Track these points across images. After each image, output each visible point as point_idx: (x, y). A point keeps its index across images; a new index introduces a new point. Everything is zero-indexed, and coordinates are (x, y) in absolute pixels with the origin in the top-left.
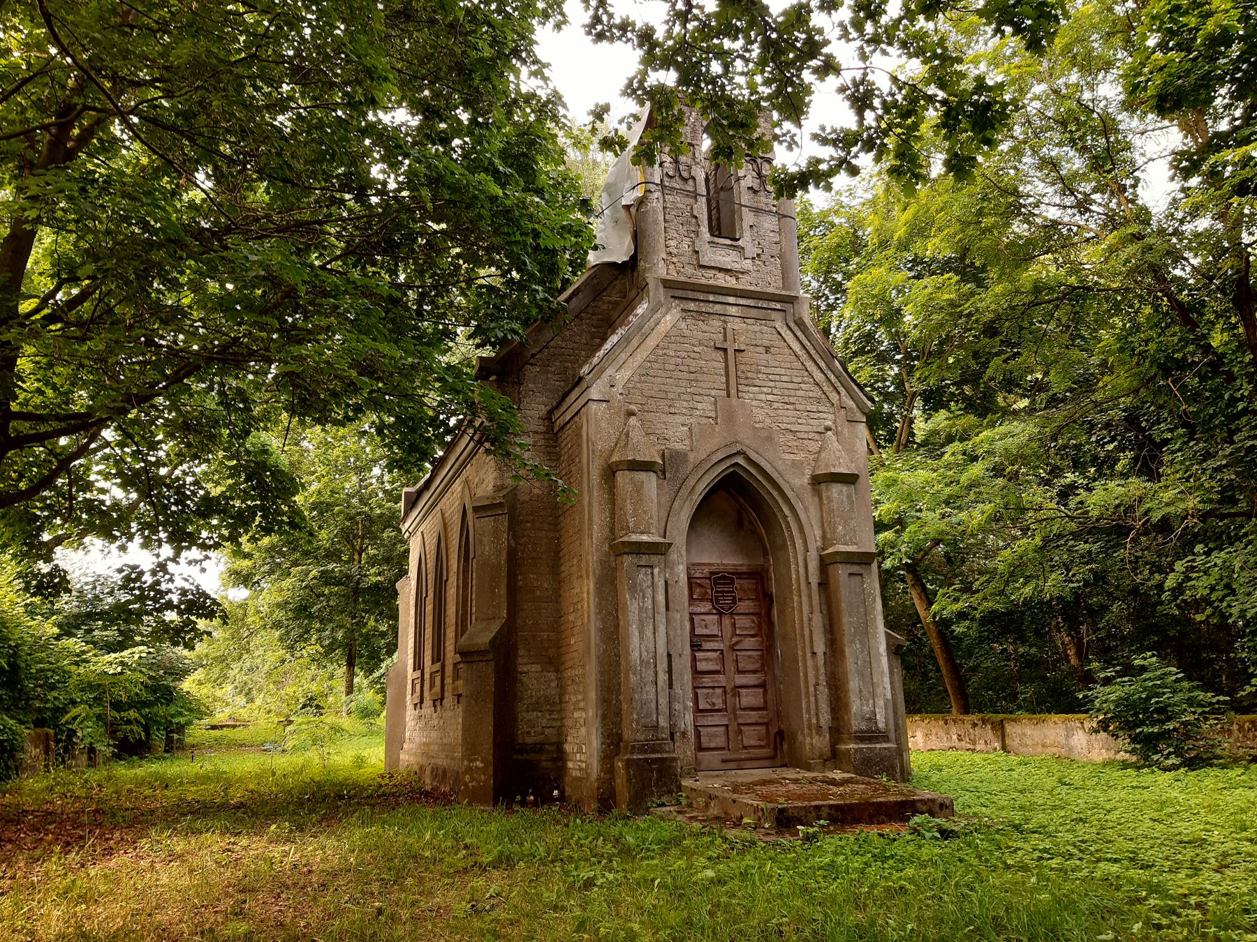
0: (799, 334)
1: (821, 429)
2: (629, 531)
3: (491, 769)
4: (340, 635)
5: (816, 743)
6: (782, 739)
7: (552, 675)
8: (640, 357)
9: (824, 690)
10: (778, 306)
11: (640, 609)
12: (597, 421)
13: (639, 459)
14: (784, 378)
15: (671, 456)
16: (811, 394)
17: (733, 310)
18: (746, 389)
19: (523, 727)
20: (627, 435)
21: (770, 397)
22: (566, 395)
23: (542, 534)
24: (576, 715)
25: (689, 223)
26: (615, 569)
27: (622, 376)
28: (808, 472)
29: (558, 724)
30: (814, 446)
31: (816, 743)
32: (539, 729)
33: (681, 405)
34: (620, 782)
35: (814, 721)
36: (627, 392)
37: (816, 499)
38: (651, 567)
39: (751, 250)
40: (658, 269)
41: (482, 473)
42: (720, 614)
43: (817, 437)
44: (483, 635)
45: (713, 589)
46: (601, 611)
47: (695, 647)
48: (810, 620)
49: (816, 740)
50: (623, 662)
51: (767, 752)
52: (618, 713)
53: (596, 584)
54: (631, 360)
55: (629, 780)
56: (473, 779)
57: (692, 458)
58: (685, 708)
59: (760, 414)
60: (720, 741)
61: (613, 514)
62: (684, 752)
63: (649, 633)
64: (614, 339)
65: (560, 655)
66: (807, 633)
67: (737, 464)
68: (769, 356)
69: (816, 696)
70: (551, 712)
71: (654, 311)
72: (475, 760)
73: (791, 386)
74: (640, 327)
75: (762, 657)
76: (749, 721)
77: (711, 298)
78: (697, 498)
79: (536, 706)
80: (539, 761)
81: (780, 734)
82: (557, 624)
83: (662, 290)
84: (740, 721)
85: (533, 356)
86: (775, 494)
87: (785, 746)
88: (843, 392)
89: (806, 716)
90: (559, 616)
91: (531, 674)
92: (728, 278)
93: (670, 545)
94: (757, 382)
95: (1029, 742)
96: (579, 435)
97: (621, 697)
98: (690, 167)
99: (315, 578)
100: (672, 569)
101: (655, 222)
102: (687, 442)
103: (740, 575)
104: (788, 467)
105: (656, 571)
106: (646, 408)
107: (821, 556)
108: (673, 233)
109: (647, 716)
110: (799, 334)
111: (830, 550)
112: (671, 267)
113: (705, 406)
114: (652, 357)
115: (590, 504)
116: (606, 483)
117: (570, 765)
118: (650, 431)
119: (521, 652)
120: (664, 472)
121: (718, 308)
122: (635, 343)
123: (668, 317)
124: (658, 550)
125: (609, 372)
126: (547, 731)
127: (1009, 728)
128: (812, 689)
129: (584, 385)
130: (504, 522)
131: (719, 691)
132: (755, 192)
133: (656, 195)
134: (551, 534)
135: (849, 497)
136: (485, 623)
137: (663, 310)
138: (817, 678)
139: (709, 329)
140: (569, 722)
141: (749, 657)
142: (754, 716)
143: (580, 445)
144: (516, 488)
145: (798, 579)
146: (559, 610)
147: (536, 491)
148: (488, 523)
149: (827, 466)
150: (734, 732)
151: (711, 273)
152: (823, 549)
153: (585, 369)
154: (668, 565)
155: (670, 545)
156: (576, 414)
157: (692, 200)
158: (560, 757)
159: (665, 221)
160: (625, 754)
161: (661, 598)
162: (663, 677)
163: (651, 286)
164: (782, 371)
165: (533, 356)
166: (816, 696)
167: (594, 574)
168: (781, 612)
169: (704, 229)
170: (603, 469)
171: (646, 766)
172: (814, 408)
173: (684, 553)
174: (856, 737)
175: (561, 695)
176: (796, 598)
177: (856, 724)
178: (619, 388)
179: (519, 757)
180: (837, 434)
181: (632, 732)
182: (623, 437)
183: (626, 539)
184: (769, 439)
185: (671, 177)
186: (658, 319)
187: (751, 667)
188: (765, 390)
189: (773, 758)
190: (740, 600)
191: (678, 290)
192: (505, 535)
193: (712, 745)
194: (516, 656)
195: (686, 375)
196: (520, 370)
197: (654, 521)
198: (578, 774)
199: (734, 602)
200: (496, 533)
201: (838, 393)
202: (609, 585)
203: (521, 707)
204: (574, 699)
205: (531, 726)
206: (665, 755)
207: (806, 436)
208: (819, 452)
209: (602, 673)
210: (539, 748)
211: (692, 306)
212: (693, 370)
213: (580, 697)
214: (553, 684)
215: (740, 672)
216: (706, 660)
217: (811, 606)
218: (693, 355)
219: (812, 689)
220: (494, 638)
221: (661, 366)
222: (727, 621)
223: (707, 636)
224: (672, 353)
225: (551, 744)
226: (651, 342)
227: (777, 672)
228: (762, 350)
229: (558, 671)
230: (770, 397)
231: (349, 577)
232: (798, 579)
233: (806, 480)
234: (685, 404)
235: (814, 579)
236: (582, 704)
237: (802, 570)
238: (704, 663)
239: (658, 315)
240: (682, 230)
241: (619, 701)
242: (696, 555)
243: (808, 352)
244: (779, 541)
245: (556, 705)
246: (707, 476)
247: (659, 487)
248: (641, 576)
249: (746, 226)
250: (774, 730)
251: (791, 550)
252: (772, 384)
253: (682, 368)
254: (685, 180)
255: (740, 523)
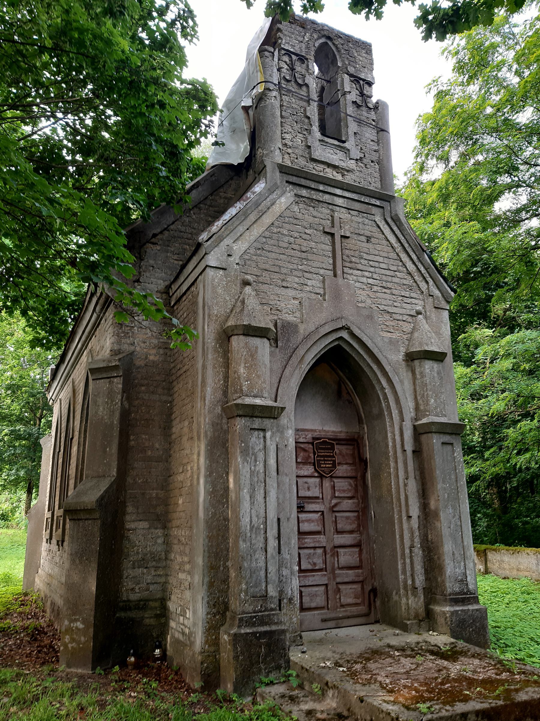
0: (395, 228)
1: (413, 313)
2: (243, 394)
3: (91, 630)
4: (22, 473)
5: (412, 603)
6: (375, 596)
7: (160, 532)
8: (257, 231)
9: (418, 552)
10: (378, 203)
11: (252, 473)
12: (214, 288)
13: (254, 324)
14: (382, 266)
15: (283, 326)
16: (405, 282)
17: (340, 201)
18: (351, 271)
19: (127, 584)
20: (243, 302)
21: (370, 281)
22: (183, 267)
23: (156, 397)
24: (182, 576)
25: (303, 122)
26: (227, 432)
27: (239, 248)
28: (403, 350)
29: (163, 580)
30: (408, 327)
31: (412, 603)
32: (144, 585)
33: (292, 280)
34: (226, 655)
35: (410, 582)
36: (244, 262)
37: (410, 374)
38: (264, 430)
39: (356, 153)
40: (274, 155)
41: (102, 342)
42: (321, 477)
43: (410, 319)
44: (92, 494)
45: (317, 453)
46: (210, 475)
47: (301, 509)
48: (405, 485)
49: (411, 600)
50: (231, 526)
51: (362, 609)
52: (226, 580)
53: (207, 445)
54: (247, 233)
55: (236, 657)
56: (73, 640)
57: (303, 329)
58: (292, 573)
59: (362, 295)
60: (320, 601)
61: (226, 377)
62: (289, 619)
63: (260, 497)
64: (232, 211)
65: (167, 513)
66: (403, 497)
67: (341, 338)
68: (370, 245)
69: (411, 557)
70: (157, 568)
71: (271, 190)
72: (76, 620)
73: (388, 273)
74: (257, 204)
75: (358, 517)
76: (346, 580)
77: (321, 188)
78: (305, 367)
79: (143, 563)
80: (143, 618)
81: (374, 591)
82: (166, 483)
83: (278, 174)
84: (338, 580)
85: (154, 235)
86: (375, 367)
87: (378, 603)
88: (431, 282)
89: (401, 577)
90: (168, 476)
91: (139, 532)
92: (335, 173)
93: (283, 409)
94: (360, 266)
95: (506, 566)
96: (195, 303)
97: (229, 564)
98: (304, 76)
99: (6, 435)
100: (282, 433)
101: (273, 115)
102: (298, 314)
103: (339, 441)
104: (387, 345)
105: (268, 434)
106: (261, 279)
107: (414, 426)
108: (288, 128)
109: (256, 586)
110: (395, 228)
111: (424, 421)
112: (286, 156)
113: (314, 283)
114: (267, 234)
115: (204, 367)
116: (221, 346)
117: (172, 624)
118: (264, 301)
119: (130, 509)
120: (276, 341)
121: (327, 197)
122: (252, 217)
123: (283, 199)
124: (271, 413)
125: (227, 241)
126: (152, 587)
127: (490, 555)
128: (407, 551)
129: (202, 252)
130: (118, 384)
131: (320, 551)
132: (359, 106)
133: (274, 93)
134: (164, 398)
135: (439, 373)
136: (95, 481)
137: (278, 192)
138: (412, 540)
139: (319, 215)
140: (172, 580)
141: (347, 518)
142: (351, 575)
143: (195, 312)
144: (132, 353)
145: (394, 446)
146: (168, 469)
147: (151, 358)
148: (104, 385)
149: (421, 344)
150: (332, 590)
151: (320, 167)
152: (416, 420)
153: (204, 236)
154: (281, 430)
155: (283, 409)
156: (193, 284)
157: (305, 104)
158: (163, 614)
159: (282, 117)
160: (232, 626)
161: (272, 462)
162: (272, 543)
163: (269, 169)
164: (381, 259)
165: (154, 235)
166: (411, 557)
167: (206, 435)
168: (376, 476)
169: (315, 128)
170: (219, 334)
171: (255, 641)
172: (407, 294)
173: (293, 418)
174: (452, 600)
175: (167, 552)
176: (392, 464)
177: (451, 587)
178: (235, 259)
179: (123, 614)
180: (426, 318)
181: (240, 603)
182: (239, 304)
183: (239, 401)
184: (370, 317)
185: (288, 81)
186: (272, 201)
187: (348, 528)
188: (367, 274)
189: (367, 615)
190: (339, 464)
191: (292, 176)
192: (119, 397)
193: (313, 605)
194: (124, 513)
195: (299, 254)
196: (141, 247)
197: (267, 386)
198: (181, 637)
199: (334, 466)
200: (110, 394)
201: (427, 282)
202: (220, 450)
203: (127, 564)
204: (179, 559)
205: (135, 583)
206: (274, 628)
207: (400, 318)
208: (412, 333)
209: (210, 538)
210: (142, 605)
211: (304, 192)
212: (304, 249)
213: (186, 559)
214: (160, 541)
215: (338, 532)
216: (309, 521)
217: (406, 472)
218: (304, 236)
219: (407, 551)
220: (102, 498)
221: (276, 242)
222: (327, 484)
223: (309, 498)
224: (286, 232)
225: (156, 600)
226: (267, 220)
227: (372, 532)
228: (364, 239)
229: (165, 527)
230: (370, 281)
231: (30, 435)
232: (394, 446)
233: (401, 356)
234: (297, 280)
235: (409, 447)
236: (187, 567)
237: (398, 438)
238: (306, 524)
239: (274, 196)
240: (297, 127)
241: (226, 568)
242: (307, 419)
243: (402, 245)
244: (375, 411)
245: (161, 562)
246: (315, 347)
247: (272, 354)
248: (253, 439)
249: (351, 132)
250: (368, 588)
251: (387, 420)
252: (372, 269)
253: (294, 246)
254: (300, 86)
255: (339, 394)
